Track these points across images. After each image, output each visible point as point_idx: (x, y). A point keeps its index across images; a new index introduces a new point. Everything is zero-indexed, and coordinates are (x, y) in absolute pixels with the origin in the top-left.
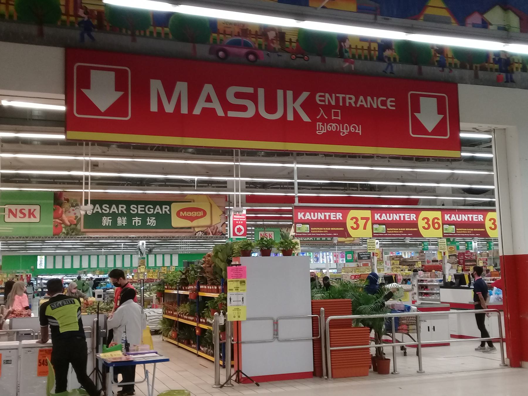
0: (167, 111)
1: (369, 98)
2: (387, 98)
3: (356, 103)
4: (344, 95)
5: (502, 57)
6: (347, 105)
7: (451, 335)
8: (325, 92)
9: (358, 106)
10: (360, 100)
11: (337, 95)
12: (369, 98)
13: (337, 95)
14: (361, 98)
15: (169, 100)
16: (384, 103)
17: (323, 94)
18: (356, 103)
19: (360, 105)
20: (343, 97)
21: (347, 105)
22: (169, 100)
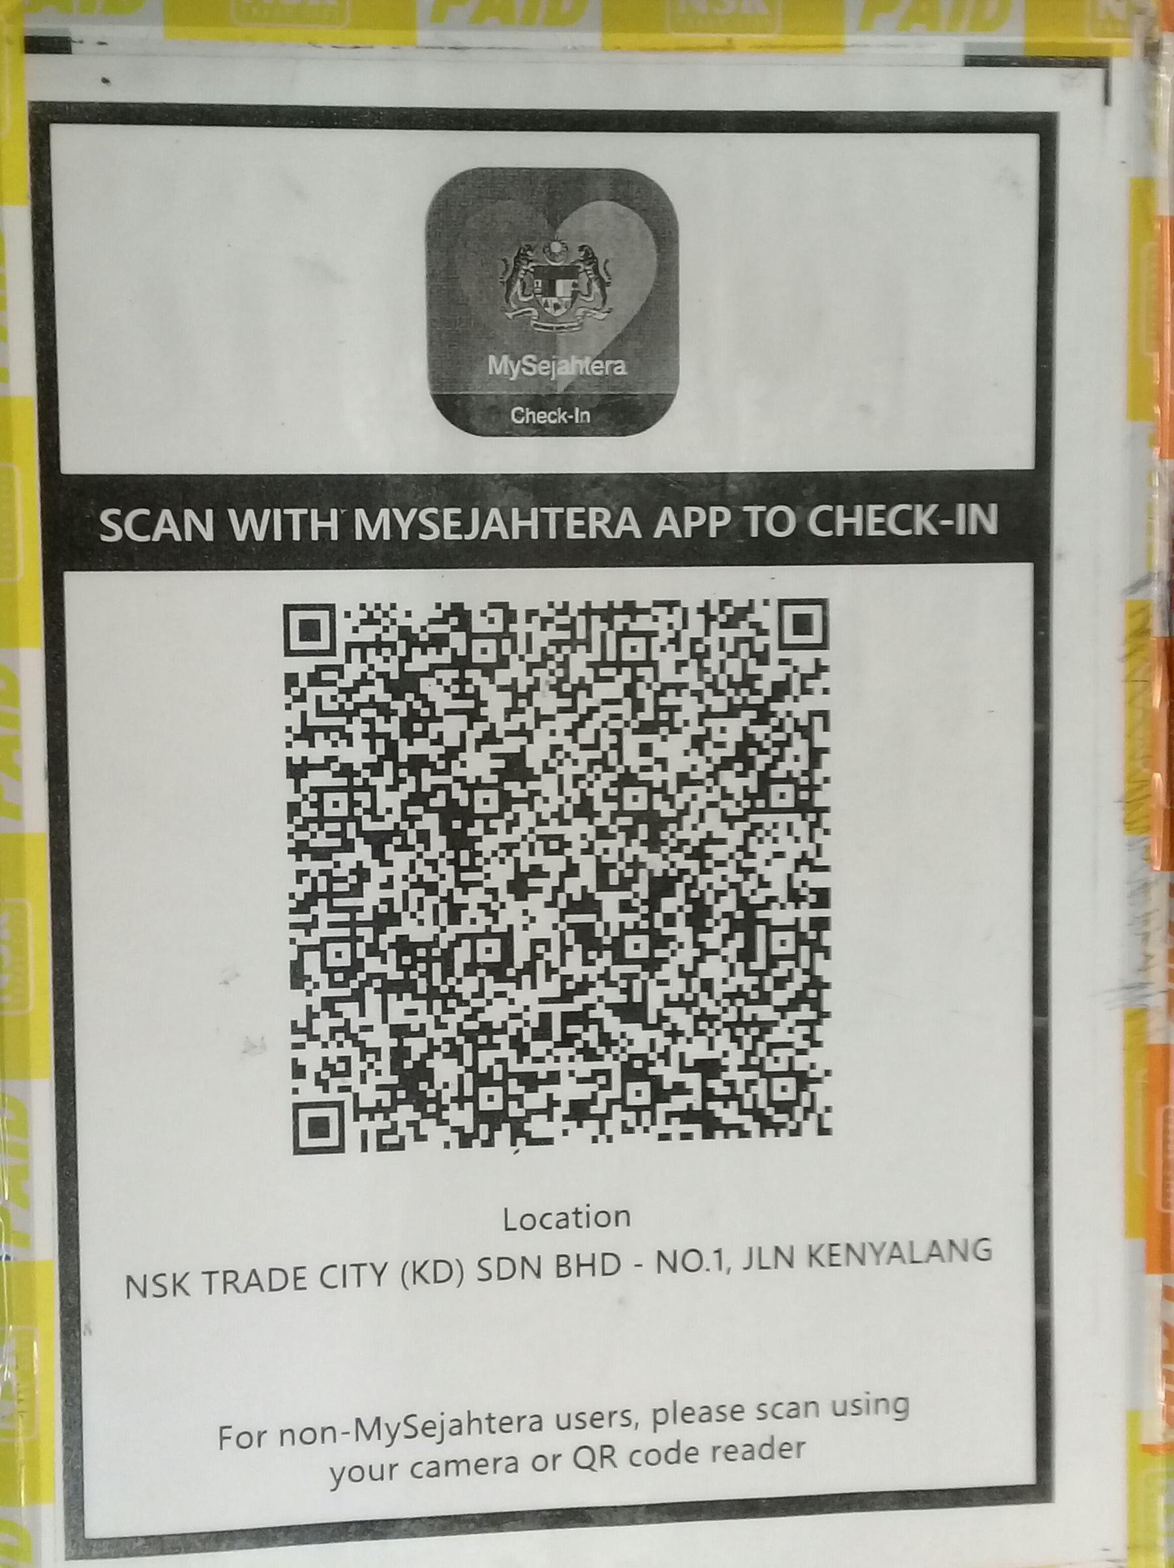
0: (239, 539)
1: (189, 514)
2: (440, 508)
3: (612, 526)
4: (561, 510)
5: (666, 1516)
6: (315, 536)
7: (68, 51)
8: (834, 505)
9: (618, 535)
10: (622, 520)
11: (287, 511)
12: (189, 514)
13: (543, 510)
14: (166, 514)
15: (373, 527)
16: (905, 520)
17: (582, 510)
18: (612, 526)
19: (163, 535)
20: (302, 516)
21: (315, 536)
22: (373, 527)
